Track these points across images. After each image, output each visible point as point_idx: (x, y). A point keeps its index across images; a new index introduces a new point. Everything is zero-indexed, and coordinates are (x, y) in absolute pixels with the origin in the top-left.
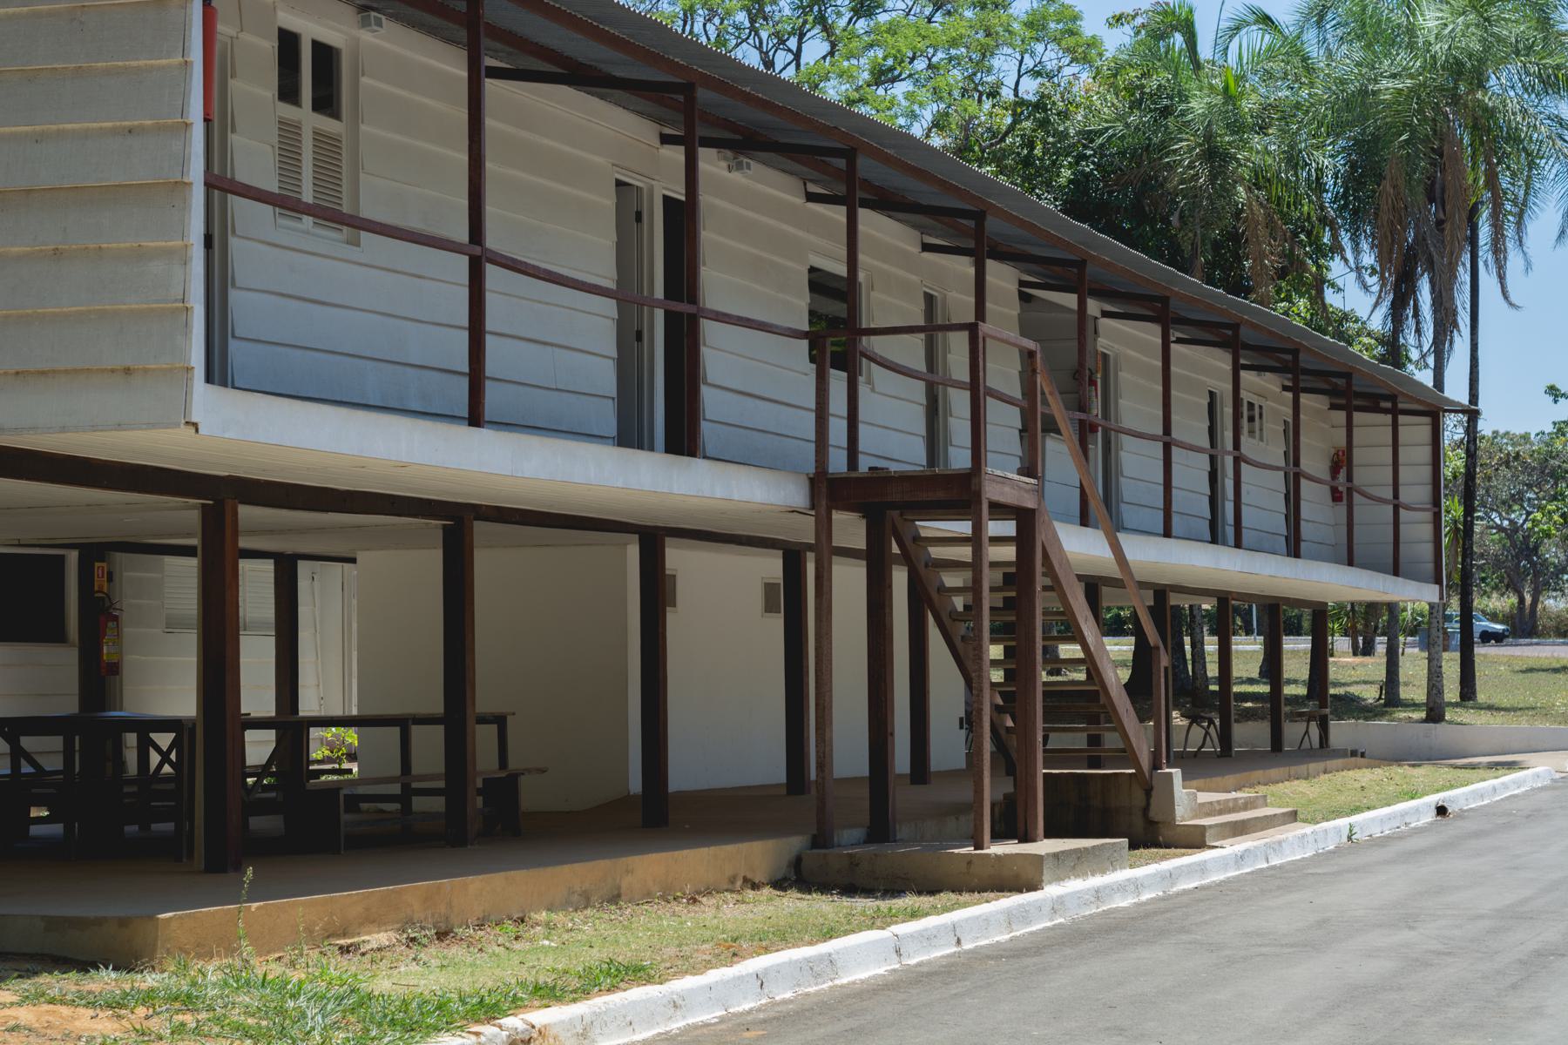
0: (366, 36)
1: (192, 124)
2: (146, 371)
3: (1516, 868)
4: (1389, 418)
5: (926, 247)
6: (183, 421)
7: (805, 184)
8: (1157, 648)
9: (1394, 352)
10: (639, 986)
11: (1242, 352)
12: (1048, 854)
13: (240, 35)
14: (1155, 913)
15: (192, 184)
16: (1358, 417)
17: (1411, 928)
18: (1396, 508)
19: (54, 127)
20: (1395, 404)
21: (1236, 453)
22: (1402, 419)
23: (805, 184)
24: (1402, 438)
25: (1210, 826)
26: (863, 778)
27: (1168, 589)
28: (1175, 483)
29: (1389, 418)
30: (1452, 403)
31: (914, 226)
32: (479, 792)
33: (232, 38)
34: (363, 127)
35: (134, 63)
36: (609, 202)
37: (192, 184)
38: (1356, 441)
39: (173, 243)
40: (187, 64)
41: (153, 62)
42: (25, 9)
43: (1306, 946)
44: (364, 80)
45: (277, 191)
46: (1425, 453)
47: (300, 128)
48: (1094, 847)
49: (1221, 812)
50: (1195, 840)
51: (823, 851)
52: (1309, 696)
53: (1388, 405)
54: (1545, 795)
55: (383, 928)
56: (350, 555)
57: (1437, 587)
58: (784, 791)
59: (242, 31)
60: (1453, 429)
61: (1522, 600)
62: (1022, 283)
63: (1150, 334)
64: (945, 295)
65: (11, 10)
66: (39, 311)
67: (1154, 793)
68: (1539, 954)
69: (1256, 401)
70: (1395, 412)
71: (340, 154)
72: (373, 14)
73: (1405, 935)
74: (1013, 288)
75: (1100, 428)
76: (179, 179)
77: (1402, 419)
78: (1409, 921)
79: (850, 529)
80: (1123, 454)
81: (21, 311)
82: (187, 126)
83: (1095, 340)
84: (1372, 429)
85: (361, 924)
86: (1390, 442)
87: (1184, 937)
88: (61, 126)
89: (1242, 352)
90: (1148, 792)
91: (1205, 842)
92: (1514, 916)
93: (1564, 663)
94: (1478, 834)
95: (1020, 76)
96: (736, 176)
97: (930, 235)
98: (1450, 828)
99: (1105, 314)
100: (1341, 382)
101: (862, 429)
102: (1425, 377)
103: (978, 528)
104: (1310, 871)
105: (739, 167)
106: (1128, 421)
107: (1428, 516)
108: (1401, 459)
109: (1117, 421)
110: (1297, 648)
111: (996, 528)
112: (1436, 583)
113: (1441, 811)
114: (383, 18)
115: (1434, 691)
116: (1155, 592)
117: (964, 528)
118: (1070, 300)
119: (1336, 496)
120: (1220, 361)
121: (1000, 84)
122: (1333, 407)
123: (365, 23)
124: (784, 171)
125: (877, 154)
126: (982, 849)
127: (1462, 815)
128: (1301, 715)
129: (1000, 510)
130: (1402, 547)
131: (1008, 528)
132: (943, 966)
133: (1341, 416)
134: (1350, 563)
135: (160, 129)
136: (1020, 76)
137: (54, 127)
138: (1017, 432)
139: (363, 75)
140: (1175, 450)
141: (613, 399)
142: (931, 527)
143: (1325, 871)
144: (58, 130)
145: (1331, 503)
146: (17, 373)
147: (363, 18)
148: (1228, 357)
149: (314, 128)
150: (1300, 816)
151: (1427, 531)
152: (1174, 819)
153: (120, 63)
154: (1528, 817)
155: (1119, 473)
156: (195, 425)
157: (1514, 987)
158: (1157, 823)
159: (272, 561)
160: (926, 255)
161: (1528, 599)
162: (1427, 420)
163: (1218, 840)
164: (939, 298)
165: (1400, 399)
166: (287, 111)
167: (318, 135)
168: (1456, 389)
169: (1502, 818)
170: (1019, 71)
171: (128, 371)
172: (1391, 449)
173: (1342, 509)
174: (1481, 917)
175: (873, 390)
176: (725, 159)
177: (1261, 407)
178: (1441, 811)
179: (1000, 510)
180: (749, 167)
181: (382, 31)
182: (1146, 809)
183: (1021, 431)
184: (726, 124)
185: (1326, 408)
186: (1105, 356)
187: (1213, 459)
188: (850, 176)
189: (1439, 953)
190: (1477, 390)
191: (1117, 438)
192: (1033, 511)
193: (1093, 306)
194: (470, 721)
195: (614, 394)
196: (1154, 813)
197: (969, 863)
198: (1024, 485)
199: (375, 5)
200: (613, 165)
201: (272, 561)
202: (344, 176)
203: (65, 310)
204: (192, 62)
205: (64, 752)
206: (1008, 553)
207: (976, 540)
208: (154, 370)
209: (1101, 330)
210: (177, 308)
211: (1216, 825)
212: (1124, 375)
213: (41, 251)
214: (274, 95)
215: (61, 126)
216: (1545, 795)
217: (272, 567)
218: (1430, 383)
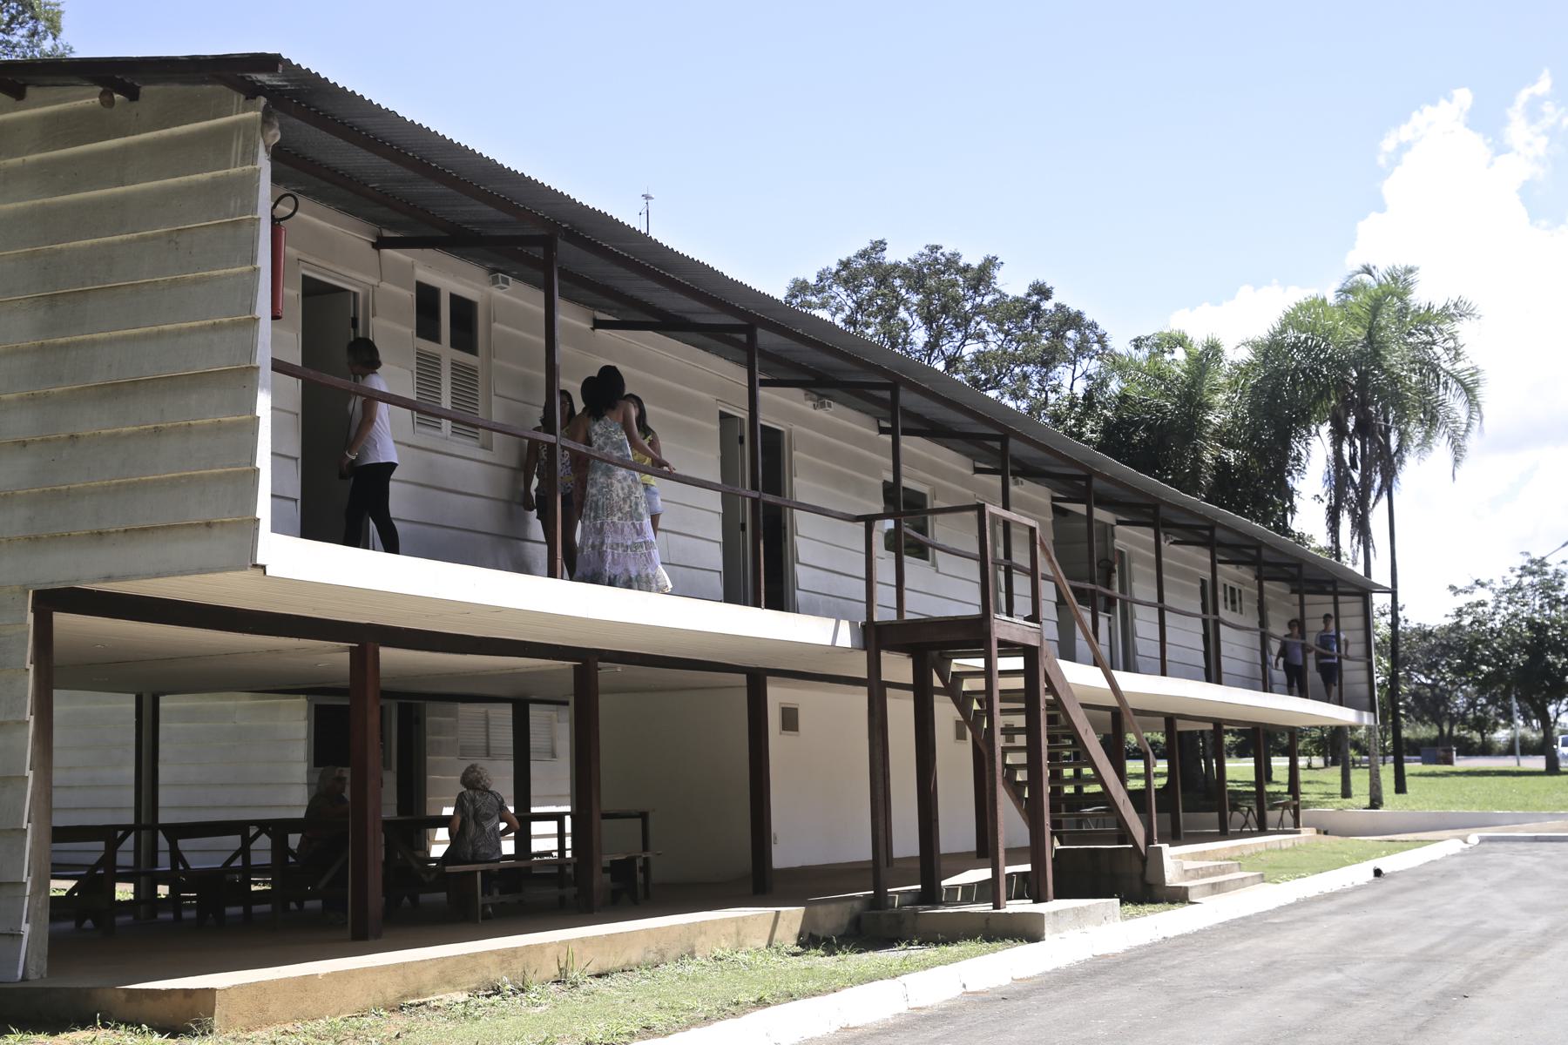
0: (497, 292)
1: (259, 318)
2: (223, 523)
3: (1430, 917)
4: (1330, 598)
5: (977, 471)
6: (250, 564)
7: (878, 421)
9: (1336, 551)
10: (1114, 955)
11: (1217, 549)
12: (1048, 913)
13: (381, 285)
14: (1136, 958)
15: (259, 367)
16: (1308, 598)
17: (1339, 971)
19: (155, 329)
20: (1335, 588)
22: (1341, 598)
23: (878, 421)
25: (1196, 886)
26: (968, 853)
28: (1168, 639)
30: (1380, 586)
31: (968, 455)
32: (605, 870)
33: (373, 286)
34: (494, 361)
35: (216, 273)
36: (715, 427)
37: (259, 367)
38: (1307, 614)
39: (244, 417)
40: (256, 271)
41: (229, 270)
42: (135, 235)
43: (1249, 988)
44: (496, 326)
46: (1358, 622)
47: (439, 360)
48: (1089, 906)
49: (1203, 877)
50: (1179, 897)
51: (879, 912)
53: (1330, 589)
54: (1457, 860)
55: (459, 988)
56: (566, 700)
57: (1372, 714)
59: (382, 281)
60: (1380, 601)
61: (1441, 731)
62: (1054, 499)
63: (1146, 535)
65: (125, 237)
66: (143, 478)
67: (1148, 862)
68: (1444, 994)
69: (1236, 585)
70: (1336, 594)
71: (477, 376)
72: (500, 275)
73: (1334, 977)
74: (1047, 502)
75: (1118, 600)
76: (248, 365)
77: (1341, 598)
78: (1336, 965)
79: (897, 667)
80: (1136, 621)
81: (129, 480)
82: (256, 320)
83: (1113, 541)
84: (1319, 605)
85: (436, 986)
87: (1151, 980)
88: (161, 327)
89: (1217, 549)
92: (1427, 959)
94: (1403, 890)
95: (1073, 380)
96: (820, 413)
97: (980, 462)
98: (1384, 886)
99: (1120, 523)
100: (1294, 571)
101: (907, 594)
102: (1360, 570)
103: (989, 663)
104: (1269, 921)
105: (823, 406)
106: (1138, 596)
107: (1363, 665)
109: (1131, 594)
110: (1280, 764)
111: (1004, 663)
113: (1378, 873)
114: (510, 279)
116: (1166, 719)
117: (979, 663)
118: (1081, 509)
120: (1202, 556)
121: (1060, 385)
122: (1293, 592)
123: (495, 282)
124: (860, 411)
125: (915, 388)
126: (999, 909)
127: (1393, 875)
128: (1278, 805)
129: (1009, 648)
131: (1017, 663)
132: (941, 1009)
133: (1296, 597)
135: (235, 324)
136: (1073, 380)
137: (155, 329)
138: (1054, 605)
139: (495, 321)
140: (1167, 613)
141: (297, 415)
142: (958, 664)
143: (1281, 920)
144: (159, 331)
146: (126, 530)
147: (493, 278)
148: (1208, 552)
149: (452, 360)
150: (1266, 877)
152: (1164, 882)
153: (206, 273)
154: (1443, 876)
155: (1134, 634)
156: (263, 567)
157: (1420, 1029)
159: (511, 705)
160: (978, 476)
161: (1446, 729)
162: (1359, 598)
163: (1199, 897)
165: (1338, 584)
166: (427, 346)
167: (456, 366)
168: (1381, 576)
169: (1424, 878)
170: (1073, 376)
171: (209, 525)
174: (1397, 960)
175: (937, 571)
176: (811, 399)
177: (1240, 591)
178: (1378, 873)
179: (1009, 648)
180: (830, 406)
181: (509, 288)
183: (1057, 604)
184: (799, 367)
185: (1288, 592)
186: (1121, 553)
187: (1205, 622)
188: (893, 406)
189: (1360, 995)
191: (1132, 607)
192: (1037, 647)
193: (1101, 514)
194: (596, 816)
195: (721, 568)
196: (1150, 878)
197: (988, 919)
198: (1028, 629)
199: (502, 268)
200: (717, 400)
201: (511, 705)
202: (480, 398)
203: (162, 476)
204: (259, 269)
206: (1019, 683)
207: (988, 673)
208: (229, 522)
209: (1116, 534)
210: (247, 471)
211: (1201, 885)
212: (1135, 566)
213: (145, 429)
214: (412, 332)
215: (161, 327)
216: (1457, 860)
217: (511, 712)
218: (1362, 573)
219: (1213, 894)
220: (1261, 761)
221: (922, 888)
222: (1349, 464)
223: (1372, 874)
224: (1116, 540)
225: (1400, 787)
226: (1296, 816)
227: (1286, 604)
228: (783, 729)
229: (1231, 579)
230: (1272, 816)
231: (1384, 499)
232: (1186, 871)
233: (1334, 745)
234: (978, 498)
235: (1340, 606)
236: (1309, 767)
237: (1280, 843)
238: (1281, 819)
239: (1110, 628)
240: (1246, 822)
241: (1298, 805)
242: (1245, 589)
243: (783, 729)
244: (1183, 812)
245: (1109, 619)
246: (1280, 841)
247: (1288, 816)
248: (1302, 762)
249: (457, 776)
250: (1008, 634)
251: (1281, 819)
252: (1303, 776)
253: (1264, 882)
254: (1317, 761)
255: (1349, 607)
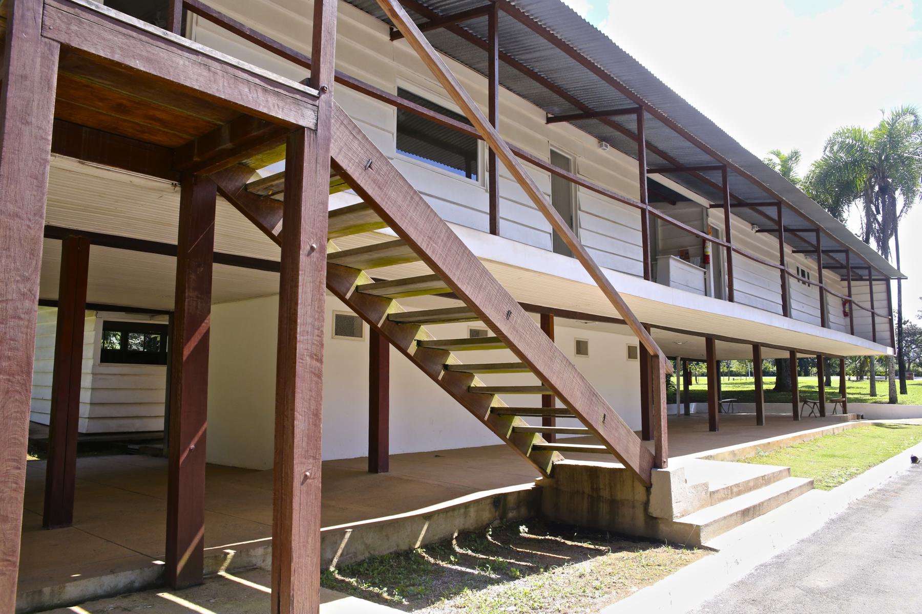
4: (868, 283)
8: (657, 356)
16: (853, 283)
18: (873, 314)
21: (782, 267)
22: (874, 283)
24: (874, 290)
27: (760, 345)
29: (868, 283)
45: (285, 160)
52: (840, 392)
58: (366, 467)
64: (576, 158)
77: (874, 283)
83: (707, 219)
86: (869, 292)
90: (648, 488)
91: (699, 542)
93: (921, 383)
99: (712, 206)
100: (841, 257)
107: (886, 320)
108: (874, 299)
112: (892, 347)
113: (914, 460)
115: (892, 391)
119: (845, 314)
130: (877, 334)
133: (845, 283)
134: (852, 334)
145: (843, 317)
151: (887, 327)
152: (671, 516)
158: (656, 518)
164: (572, 160)
172: (869, 287)
173: (848, 319)
177: (808, 273)
182: (646, 504)
185: (840, 280)
190: (901, 283)
196: (654, 510)
205: (165, 416)
209: (710, 214)
219: (744, 522)
220: (713, 380)
221: (273, 539)
222: (875, 213)
223: (910, 460)
224: (709, 219)
225: (904, 391)
226: (844, 407)
227: (838, 286)
228: (629, 358)
229: (801, 264)
230: (829, 406)
231: (893, 237)
232: (712, 493)
233: (864, 367)
234: (552, 145)
235: (873, 287)
236: (849, 380)
237: (833, 431)
238: (835, 408)
239: (705, 279)
240: (813, 412)
241: (845, 401)
242: (811, 273)
243: (629, 358)
244: (765, 402)
245: (705, 273)
246: (833, 429)
247: (839, 407)
248: (847, 378)
249: (441, 372)
250: (148, 60)
251: (835, 408)
252: (848, 384)
253: (813, 488)
254: (854, 378)
255: (879, 287)
